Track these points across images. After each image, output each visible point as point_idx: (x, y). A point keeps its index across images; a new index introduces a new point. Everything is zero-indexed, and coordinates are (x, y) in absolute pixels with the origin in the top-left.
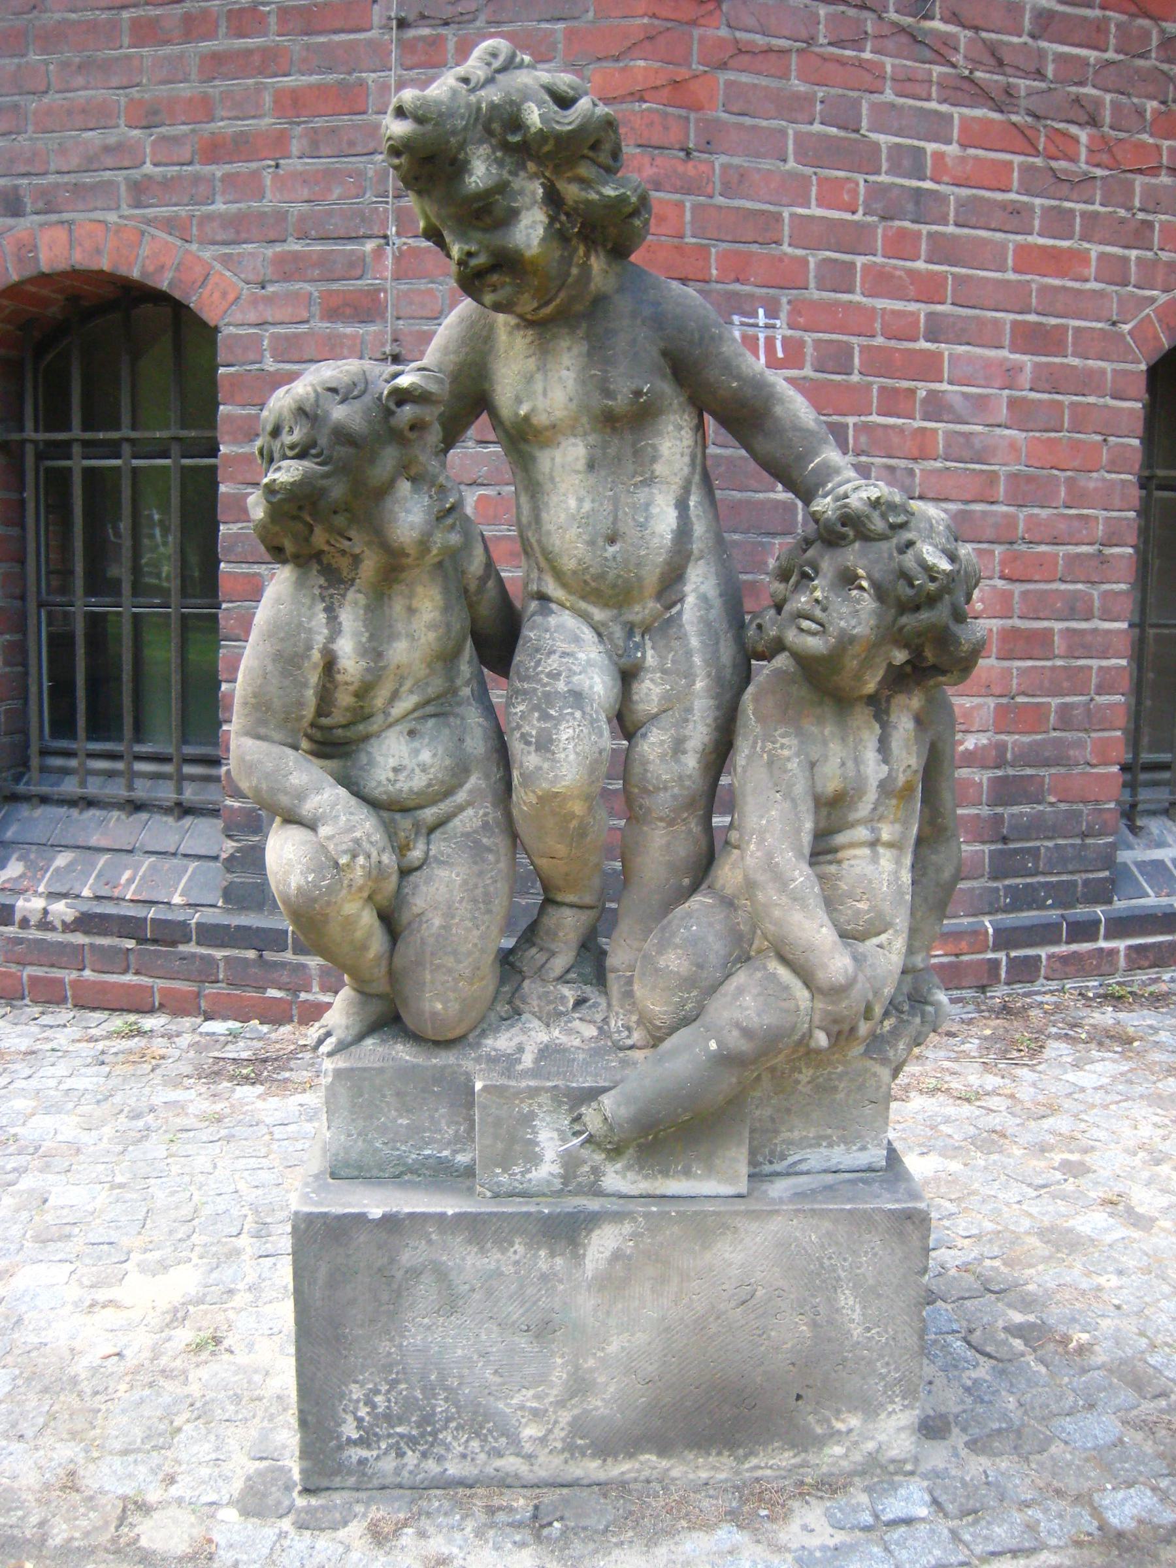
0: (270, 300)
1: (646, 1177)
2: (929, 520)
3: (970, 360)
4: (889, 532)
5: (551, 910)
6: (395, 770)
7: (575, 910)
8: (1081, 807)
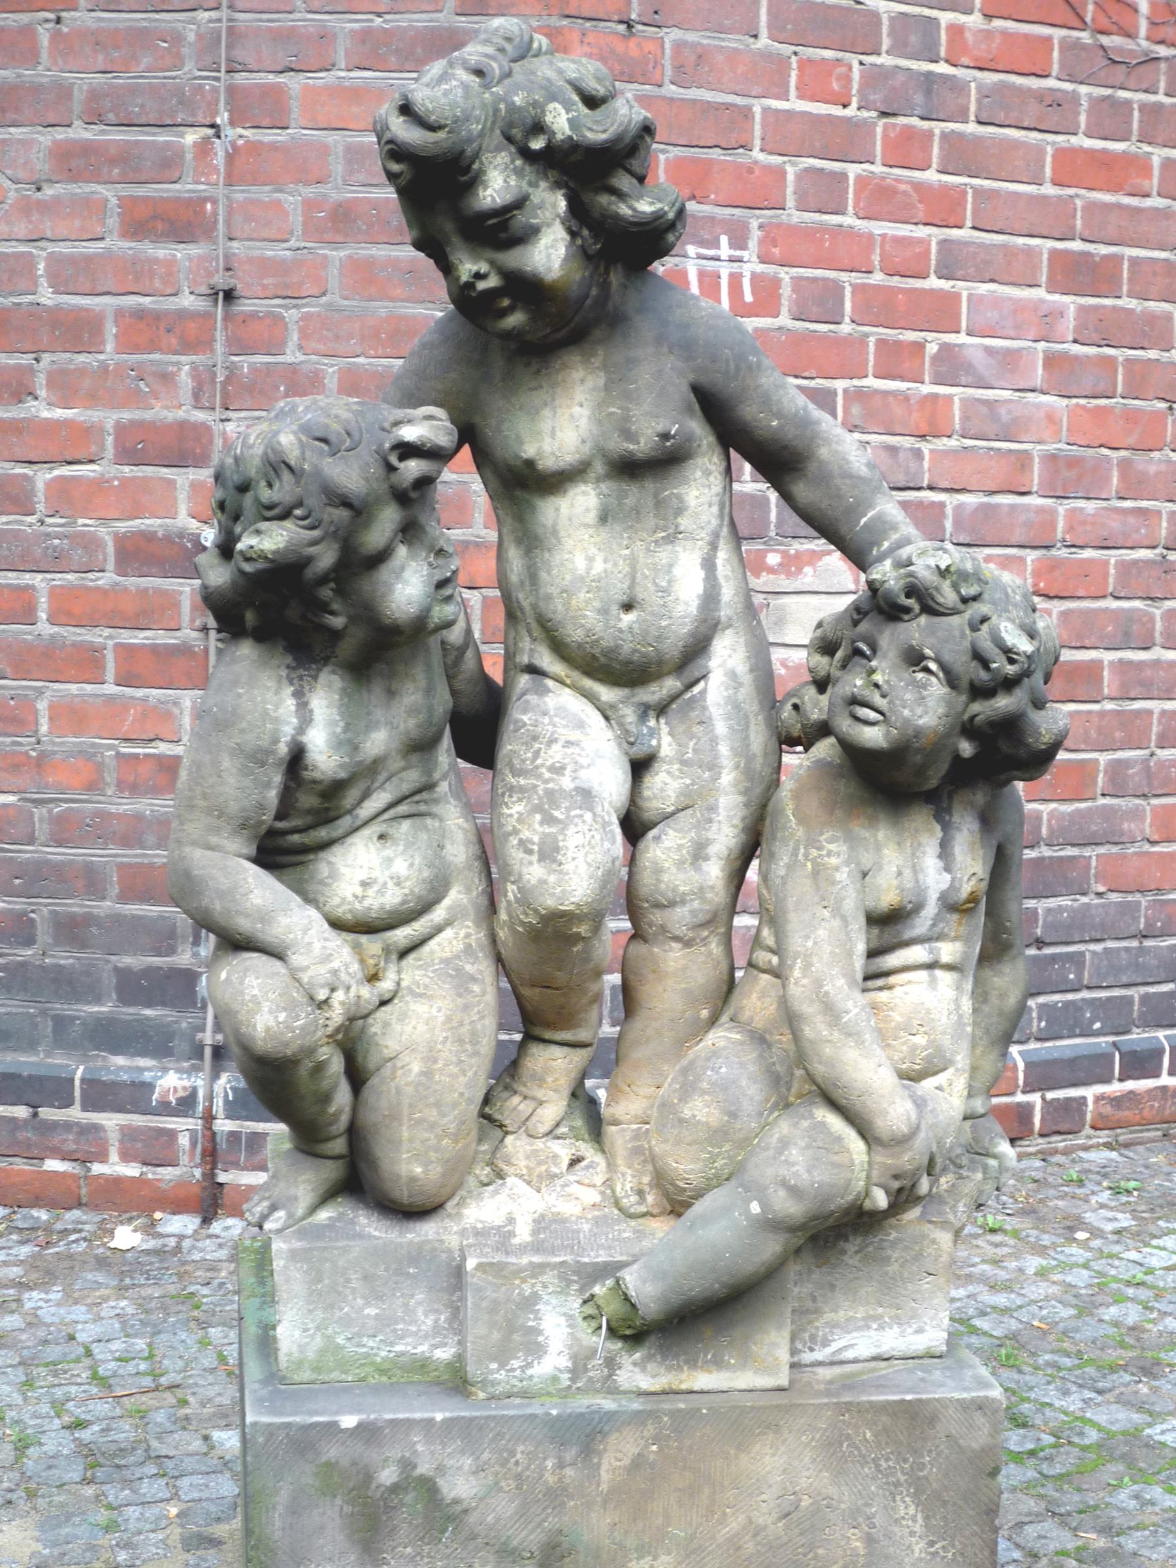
0: (45, 207)
1: (669, 1369)
2: (1004, 589)
3: (996, 302)
4: (961, 606)
5: (535, 1049)
6: (364, 884)
7: (566, 1049)
8: (1138, 897)
